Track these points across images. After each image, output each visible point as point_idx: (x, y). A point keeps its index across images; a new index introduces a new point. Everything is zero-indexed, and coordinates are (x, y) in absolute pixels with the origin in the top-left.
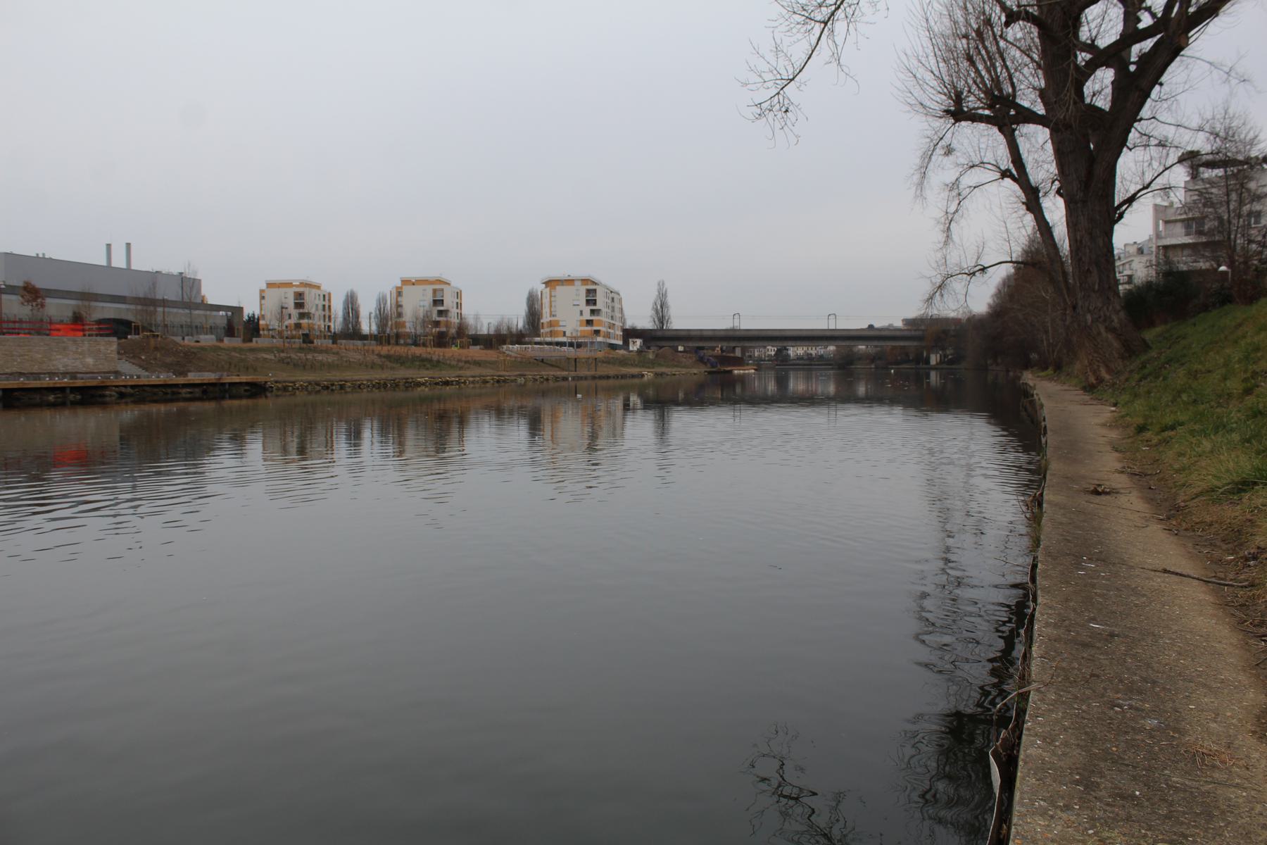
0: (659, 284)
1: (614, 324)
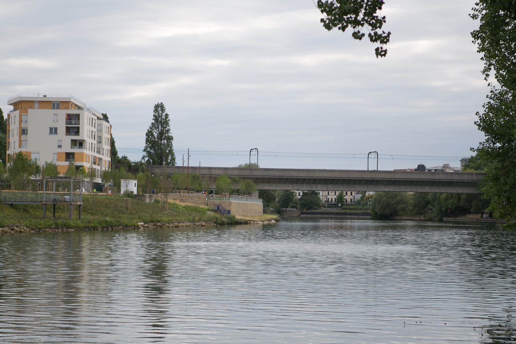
0: (156, 110)
1: (100, 159)
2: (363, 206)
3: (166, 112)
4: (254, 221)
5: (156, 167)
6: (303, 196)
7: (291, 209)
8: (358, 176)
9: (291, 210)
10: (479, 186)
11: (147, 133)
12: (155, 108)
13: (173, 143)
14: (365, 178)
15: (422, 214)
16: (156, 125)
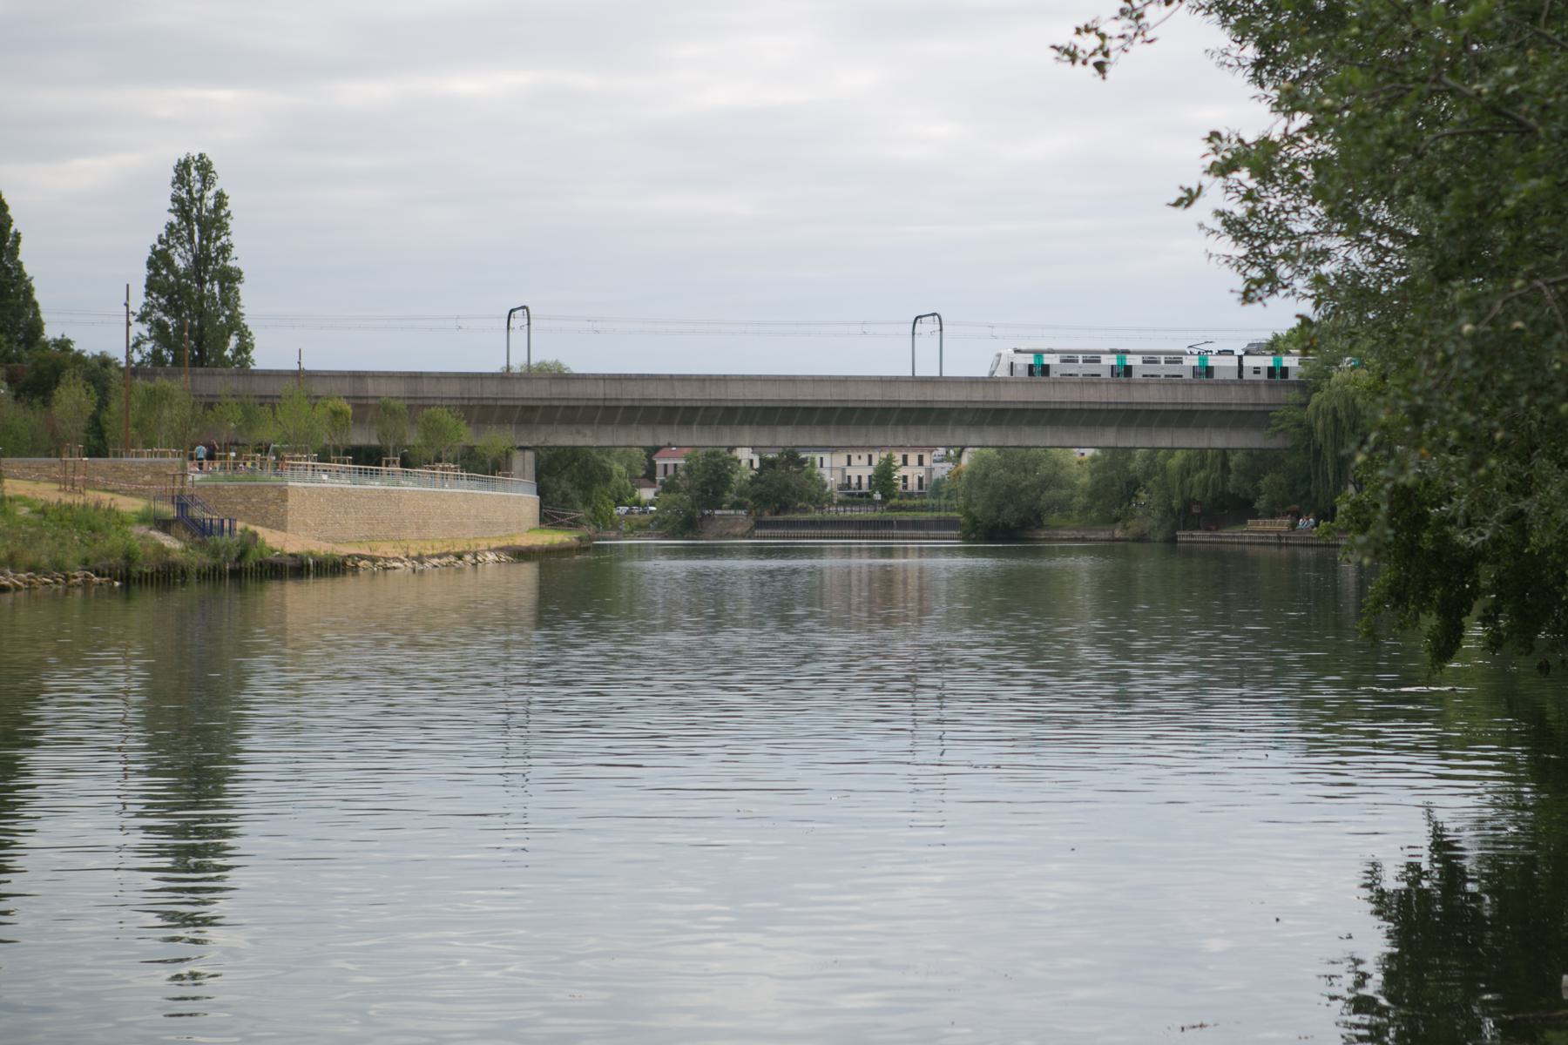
2: (948, 497)
3: (219, 185)
4: (373, 560)
5: (201, 374)
6: (761, 470)
7: (732, 512)
8: (874, 395)
9: (730, 515)
10: (1278, 425)
11: (150, 258)
12: (176, 171)
13: (240, 294)
14: (899, 401)
15: (1117, 520)
16: (184, 229)
